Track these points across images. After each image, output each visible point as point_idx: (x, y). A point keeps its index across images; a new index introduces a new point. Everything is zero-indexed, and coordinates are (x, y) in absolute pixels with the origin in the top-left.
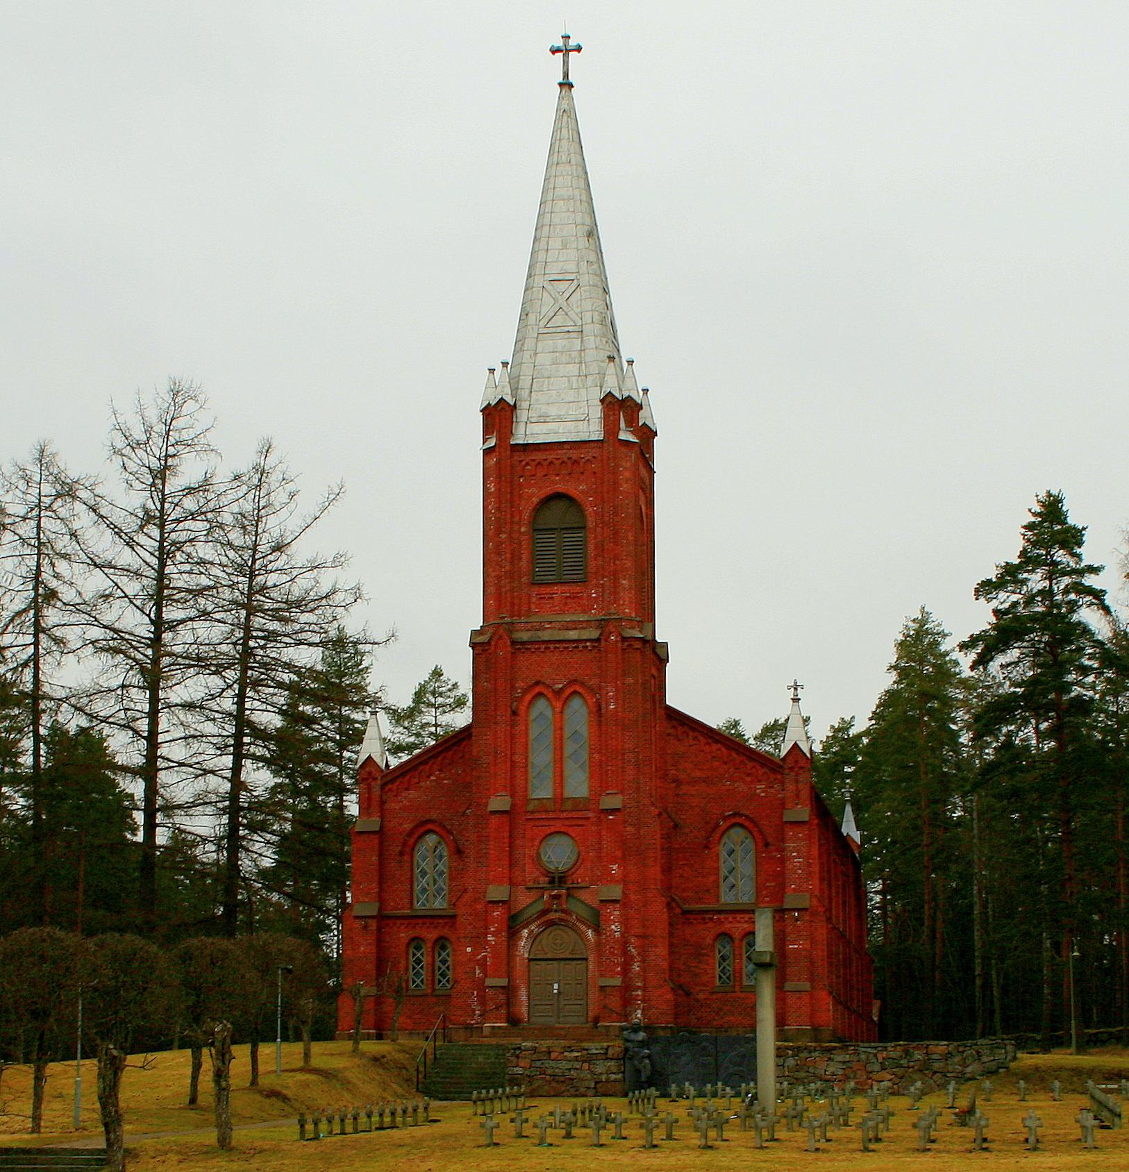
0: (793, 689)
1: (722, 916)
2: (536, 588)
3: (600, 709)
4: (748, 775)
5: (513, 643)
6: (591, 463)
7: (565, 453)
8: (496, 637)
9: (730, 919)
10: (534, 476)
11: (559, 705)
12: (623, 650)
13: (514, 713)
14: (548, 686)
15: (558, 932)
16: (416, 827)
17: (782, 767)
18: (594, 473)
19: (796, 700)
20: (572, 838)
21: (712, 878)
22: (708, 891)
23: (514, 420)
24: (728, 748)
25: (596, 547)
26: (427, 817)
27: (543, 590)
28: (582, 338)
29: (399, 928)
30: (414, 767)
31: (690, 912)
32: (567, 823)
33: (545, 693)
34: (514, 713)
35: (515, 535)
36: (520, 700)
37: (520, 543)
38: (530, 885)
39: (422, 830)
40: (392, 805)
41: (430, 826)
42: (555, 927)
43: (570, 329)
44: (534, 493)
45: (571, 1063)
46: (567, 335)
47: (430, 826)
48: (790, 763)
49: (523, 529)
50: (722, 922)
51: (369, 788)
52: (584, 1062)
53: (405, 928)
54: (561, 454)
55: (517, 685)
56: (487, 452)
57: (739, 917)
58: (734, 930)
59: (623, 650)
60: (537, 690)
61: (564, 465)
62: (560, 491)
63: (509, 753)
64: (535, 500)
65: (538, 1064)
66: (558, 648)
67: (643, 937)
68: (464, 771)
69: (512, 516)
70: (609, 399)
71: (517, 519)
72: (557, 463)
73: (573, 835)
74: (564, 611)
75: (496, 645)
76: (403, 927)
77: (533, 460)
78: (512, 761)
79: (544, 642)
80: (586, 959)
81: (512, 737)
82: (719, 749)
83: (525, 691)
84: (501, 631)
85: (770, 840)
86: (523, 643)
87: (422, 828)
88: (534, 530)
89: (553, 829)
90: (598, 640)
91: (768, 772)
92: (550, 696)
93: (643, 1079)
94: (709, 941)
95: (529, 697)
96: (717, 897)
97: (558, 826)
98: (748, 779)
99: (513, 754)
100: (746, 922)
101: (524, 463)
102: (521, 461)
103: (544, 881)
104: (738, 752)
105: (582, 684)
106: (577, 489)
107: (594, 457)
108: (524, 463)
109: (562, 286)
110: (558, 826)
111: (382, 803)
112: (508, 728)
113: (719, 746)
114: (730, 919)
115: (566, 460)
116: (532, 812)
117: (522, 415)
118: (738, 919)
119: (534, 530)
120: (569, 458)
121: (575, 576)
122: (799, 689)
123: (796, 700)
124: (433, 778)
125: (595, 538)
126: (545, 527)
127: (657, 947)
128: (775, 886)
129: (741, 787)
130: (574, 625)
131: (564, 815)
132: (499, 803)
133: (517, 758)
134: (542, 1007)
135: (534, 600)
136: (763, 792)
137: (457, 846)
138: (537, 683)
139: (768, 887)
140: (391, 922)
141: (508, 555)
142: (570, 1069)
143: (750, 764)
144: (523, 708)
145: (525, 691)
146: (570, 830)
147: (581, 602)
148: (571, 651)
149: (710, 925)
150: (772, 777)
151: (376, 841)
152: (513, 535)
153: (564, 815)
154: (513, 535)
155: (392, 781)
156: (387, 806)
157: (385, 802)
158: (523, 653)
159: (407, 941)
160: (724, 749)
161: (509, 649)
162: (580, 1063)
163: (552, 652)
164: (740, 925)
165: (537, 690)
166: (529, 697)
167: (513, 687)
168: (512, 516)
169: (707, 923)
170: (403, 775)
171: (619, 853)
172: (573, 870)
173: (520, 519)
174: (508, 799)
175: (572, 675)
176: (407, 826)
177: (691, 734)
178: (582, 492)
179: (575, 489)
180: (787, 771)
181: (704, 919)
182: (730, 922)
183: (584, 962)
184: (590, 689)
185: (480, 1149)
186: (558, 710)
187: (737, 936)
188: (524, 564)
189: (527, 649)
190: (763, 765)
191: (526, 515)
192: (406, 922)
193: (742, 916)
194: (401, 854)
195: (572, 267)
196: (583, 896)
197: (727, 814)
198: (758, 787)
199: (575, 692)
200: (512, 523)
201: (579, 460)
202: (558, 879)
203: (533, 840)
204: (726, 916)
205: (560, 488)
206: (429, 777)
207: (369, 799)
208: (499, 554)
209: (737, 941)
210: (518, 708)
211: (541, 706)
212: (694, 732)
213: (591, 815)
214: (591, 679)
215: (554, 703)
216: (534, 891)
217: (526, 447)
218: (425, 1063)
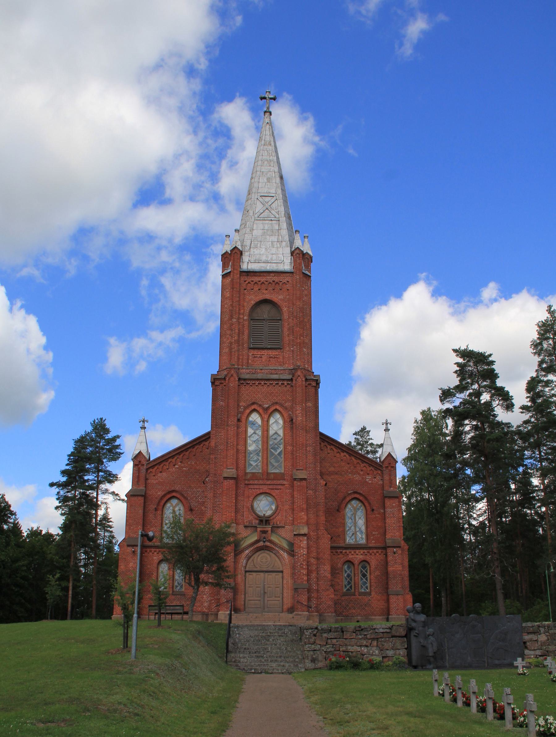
0: (385, 425)
1: (348, 551)
2: (252, 351)
3: (292, 420)
4: (362, 470)
5: (240, 379)
6: (286, 284)
7: (271, 279)
8: (230, 375)
9: (353, 553)
10: (252, 289)
11: (266, 417)
12: (306, 386)
13: (239, 420)
14: (260, 405)
15: (263, 554)
16: (164, 496)
17: (381, 466)
18: (288, 290)
19: (387, 430)
20: (274, 497)
21: (341, 529)
22: (339, 536)
23: (241, 261)
24: (350, 455)
25: (289, 329)
26: (173, 489)
27: (255, 352)
28: (279, 224)
29: (153, 553)
30: (166, 459)
32: (271, 487)
33: (258, 409)
34: (239, 420)
35: (241, 321)
36: (242, 413)
37: (244, 327)
38: (247, 524)
39: (169, 496)
40: (152, 481)
41: (174, 494)
42: (262, 551)
43: (273, 219)
44: (252, 298)
46: (271, 222)
47: (174, 494)
48: (386, 464)
49: (245, 318)
50: (348, 554)
51: (139, 469)
53: (158, 553)
54: (270, 278)
55: (240, 404)
56: (224, 276)
57: (357, 551)
58: (355, 559)
59: (306, 386)
60: (253, 407)
61: (270, 285)
62: (268, 298)
63: (235, 443)
64: (253, 302)
66: (266, 384)
67: (318, 559)
68: (196, 463)
69: (239, 310)
70: (297, 251)
71: (242, 311)
72: (266, 283)
73: (274, 495)
74: (269, 365)
75: (229, 379)
76: (155, 553)
77: (252, 281)
78: (237, 449)
79: (258, 380)
80: (282, 572)
81: (238, 435)
82: (345, 456)
83: (246, 408)
84: (233, 372)
85: (374, 508)
86: (245, 380)
87: (170, 495)
88: (251, 319)
89: (261, 491)
90: (292, 380)
91: (373, 469)
92: (261, 411)
93: (431, 655)
94: (339, 565)
95: (248, 411)
96: (345, 540)
97: (265, 489)
98: (362, 473)
99: (237, 445)
100: (362, 554)
101: (247, 282)
102: (245, 281)
103: (255, 522)
104: (356, 458)
105: (282, 405)
106: (277, 298)
107: (288, 282)
108: (247, 282)
109: (267, 199)
110: (265, 489)
111: (146, 479)
112: (236, 428)
113: (345, 454)
114: (353, 553)
115: (271, 282)
116: (249, 480)
117: (245, 258)
118: (357, 553)
119: (251, 319)
120: (274, 281)
121: (276, 346)
122: (388, 424)
123: (387, 430)
124: (176, 466)
125: (288, 324)
126: (258, 318)
127: (325, 565)
128: (378, 534)
129: (357, 477)
130: (276, 372)
131: (269, 482)
132: (231, 472)
133: (240, 447)
134: (254, 602)
135: (251, 358)
136: (370, 480)
137: (190, 506)
138: (253, 403)
139: (374, 535)
140: (148, 550)
141: (237, 331)
143: (362, 465)
144: (244, 418)
145: (246, 408)
146: (272, 492)
147: (279, 360)
148: (274, 386)
149: (341, 556)
150: (375, 472)
151: (143, 501)
152: (240, 321)
153: (269, 482)
154: (240, 321)
155: (153, 467)
156: (149, 481)
157: (148, 479)
158: (245, 386)
159: (157, 562)
160: (347, 456)
161: (237, 382)
162: (370, 641)
163: (263, 386)
164: (358, 556)
165: (253, 407)
166: (248, 411)
167: (238, 406)
168: (239, 310)
169: (339, 555)
170: (159, 463)
171: (304, 506)
172: (274, 516)
173: (244, 312)
174: (234, 471)
175: (274, 400)
176: (160, 493)
177: (329, 447)
178: (281, 300)
179: (276, 298)
180: (384, 469)
181: (337, 552)
182: (352, 555)
183: (281, 574)
184: (286, 408)
186: (266, 419)
187: (356, 562)
188: (246, 337)
189: (247, 383)
190: (370, 465)
191: (247, 310)
192: (157, 550)
193: (359, 551)
194: (156, 509)
195: (273, 191)
196: (282, 532)
197: (349, 492)
198: (367, 477)
199: (276, 410)
200: (239, 314)
201: (279, 282)
202: (264, 521)
203: (249, 497)
204: (350, 551)
205: (268, 297)
206: (174, 465)
207: (138, 477)
208: (231, 330)
209: (356, 566)
210: (241, 417)
212: (330, 446)
213: (285, 482)
214: (286, 402)
215: (263, 416)
217: (249, 273)
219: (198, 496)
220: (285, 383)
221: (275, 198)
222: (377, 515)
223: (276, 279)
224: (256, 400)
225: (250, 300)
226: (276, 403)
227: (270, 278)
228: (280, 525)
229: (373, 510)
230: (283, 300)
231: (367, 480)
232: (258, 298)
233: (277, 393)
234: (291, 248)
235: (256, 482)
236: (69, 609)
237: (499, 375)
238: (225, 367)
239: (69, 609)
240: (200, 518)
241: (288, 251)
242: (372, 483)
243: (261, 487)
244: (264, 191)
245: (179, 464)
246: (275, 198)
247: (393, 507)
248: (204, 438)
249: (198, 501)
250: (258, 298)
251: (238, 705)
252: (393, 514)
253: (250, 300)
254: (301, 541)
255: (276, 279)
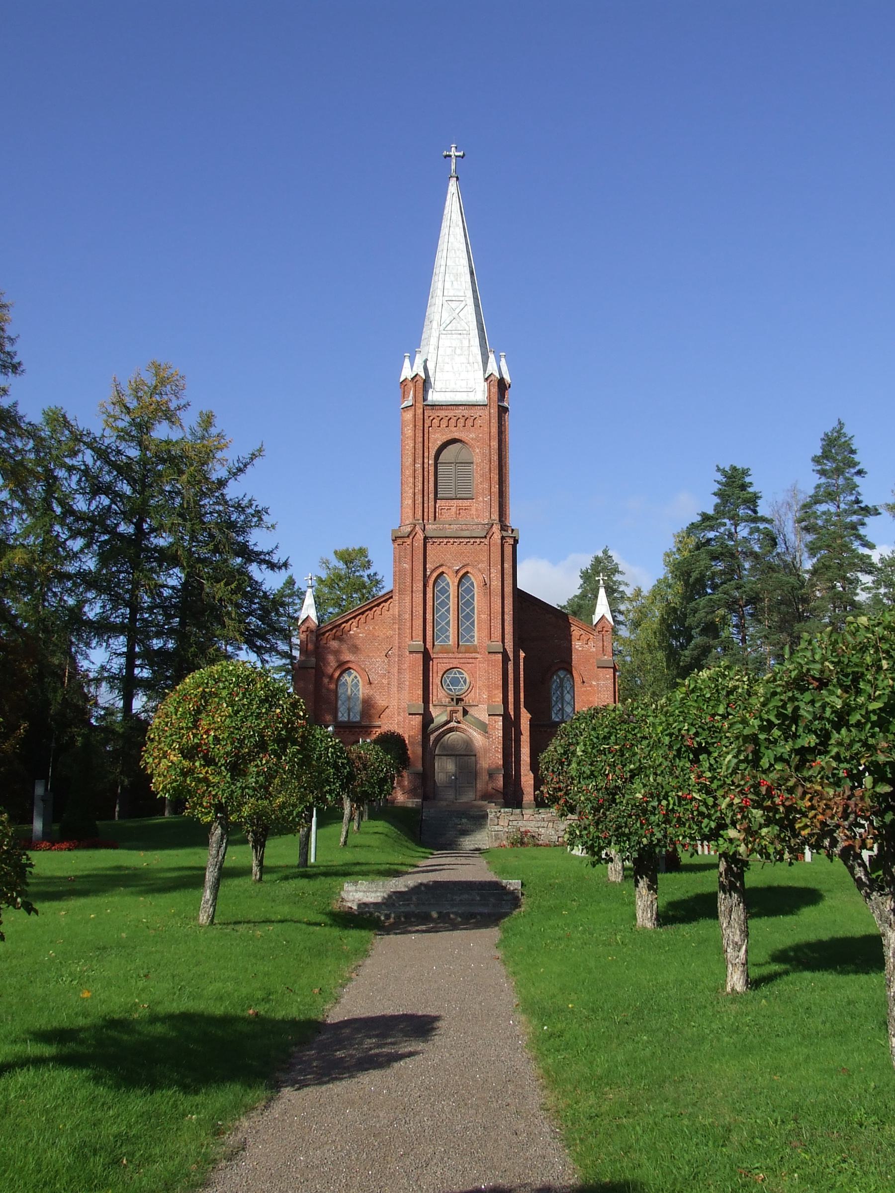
7: (461, 413)
31: (345, 842)
32: (462, 661)
45: (540, 823)
46: (459, 336)
52: (549, 821)
54: (459, 412)
65: (515, 823)
77: (438, 416)
109: (453, 305)
115: (461, 417)
131: (460, 655)
142: (538, 827)
172: (466, 694)
178: (472, 439)
185: (368, 844)
205: (456, 435)
211: (342, 893)
216: (438, 707)
218: (309, 924)
219: (378, 667)
220: (478, 540)
221: (464, 303)
222: (588, 689)
223: (466, 413)
224: (444, 561)
225: (436, 440)
226: (468, 565)
227: (459, 412)
228: (472, 704)
229: (583, 682)
230: (475, 439)
231: (577, 647)
232: (444, 437)
233: (469, 552)
234: (485, 371)
235: (445, 655)
236: (314, 819)
237: (822, 436)
238: (407, 522)
239: (314, 819)
240: (380, 692)
241: (480, 376)
242: (582, 650)
243: (452, 661)
244: (450, 292)
245: (355, 629)
246: (464, 303)
247: (607, 679)
248: (384, 599)
249: (378, 673)
250: (444, 437)
251: (250, 456)
252: (606, 687)
253: (436, 440)
254: (495, 722)
255: (466, 413)
